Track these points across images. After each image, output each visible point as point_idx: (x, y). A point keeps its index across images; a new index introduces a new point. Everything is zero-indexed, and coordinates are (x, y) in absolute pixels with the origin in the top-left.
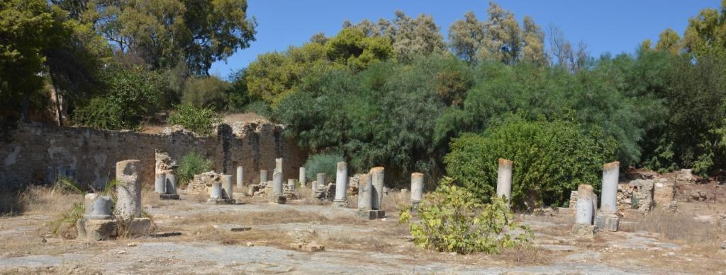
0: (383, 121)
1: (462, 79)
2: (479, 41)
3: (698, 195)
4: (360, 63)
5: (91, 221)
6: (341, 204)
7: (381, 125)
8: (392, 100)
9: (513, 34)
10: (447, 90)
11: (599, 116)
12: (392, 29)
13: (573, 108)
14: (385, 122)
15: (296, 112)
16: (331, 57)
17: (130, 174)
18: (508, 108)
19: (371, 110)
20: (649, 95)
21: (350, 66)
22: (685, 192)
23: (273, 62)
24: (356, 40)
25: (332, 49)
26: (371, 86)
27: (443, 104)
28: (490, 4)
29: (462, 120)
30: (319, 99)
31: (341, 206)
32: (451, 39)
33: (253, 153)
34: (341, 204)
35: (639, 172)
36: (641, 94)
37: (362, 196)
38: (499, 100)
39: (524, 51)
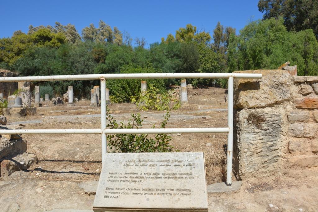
0: (69, 70)
1: (103, 51)
2: (95, 36)
3: (195, 93)
4: (51, 44)
5: (14, 109)
6: (72, 104)
7: (68, 72)
8: (73, 61)
9: (110, 34)
10: (97, 56)
11: (159, 65)
12: (55, 30)
13: (150, 62)
14: (70, 71)
15: (25, 66)
16: (36, 41)
17: (27, 87)
18: (125, 63)
19: (63, 65)
20: (175, 57)
21: (46, 46)
22: (191, 92)
23: (7, 43)
24: (48, 34)
25: (37, 38)
26: (62, 55)
27: (96, 62)
28: (100, 21)
29: (105, 68)
30: (36, 60)
31: (72, 105)
32: (83, 35)
33: (3, 87)
34: (72, 104)
35: (174, 86)
36: (172, 57)
37: (93, 98)
38: (120, 60)
39: (115, 41)
